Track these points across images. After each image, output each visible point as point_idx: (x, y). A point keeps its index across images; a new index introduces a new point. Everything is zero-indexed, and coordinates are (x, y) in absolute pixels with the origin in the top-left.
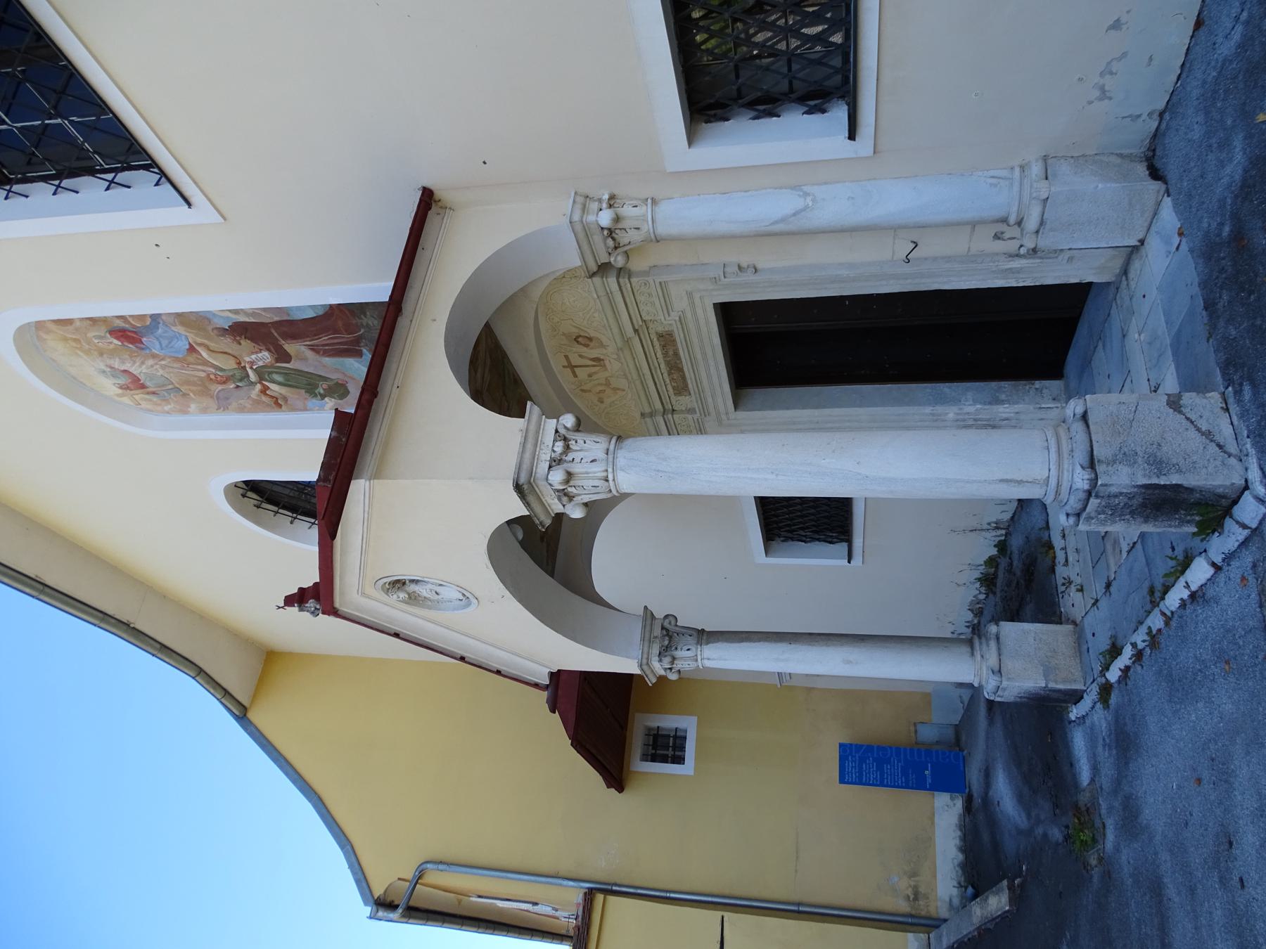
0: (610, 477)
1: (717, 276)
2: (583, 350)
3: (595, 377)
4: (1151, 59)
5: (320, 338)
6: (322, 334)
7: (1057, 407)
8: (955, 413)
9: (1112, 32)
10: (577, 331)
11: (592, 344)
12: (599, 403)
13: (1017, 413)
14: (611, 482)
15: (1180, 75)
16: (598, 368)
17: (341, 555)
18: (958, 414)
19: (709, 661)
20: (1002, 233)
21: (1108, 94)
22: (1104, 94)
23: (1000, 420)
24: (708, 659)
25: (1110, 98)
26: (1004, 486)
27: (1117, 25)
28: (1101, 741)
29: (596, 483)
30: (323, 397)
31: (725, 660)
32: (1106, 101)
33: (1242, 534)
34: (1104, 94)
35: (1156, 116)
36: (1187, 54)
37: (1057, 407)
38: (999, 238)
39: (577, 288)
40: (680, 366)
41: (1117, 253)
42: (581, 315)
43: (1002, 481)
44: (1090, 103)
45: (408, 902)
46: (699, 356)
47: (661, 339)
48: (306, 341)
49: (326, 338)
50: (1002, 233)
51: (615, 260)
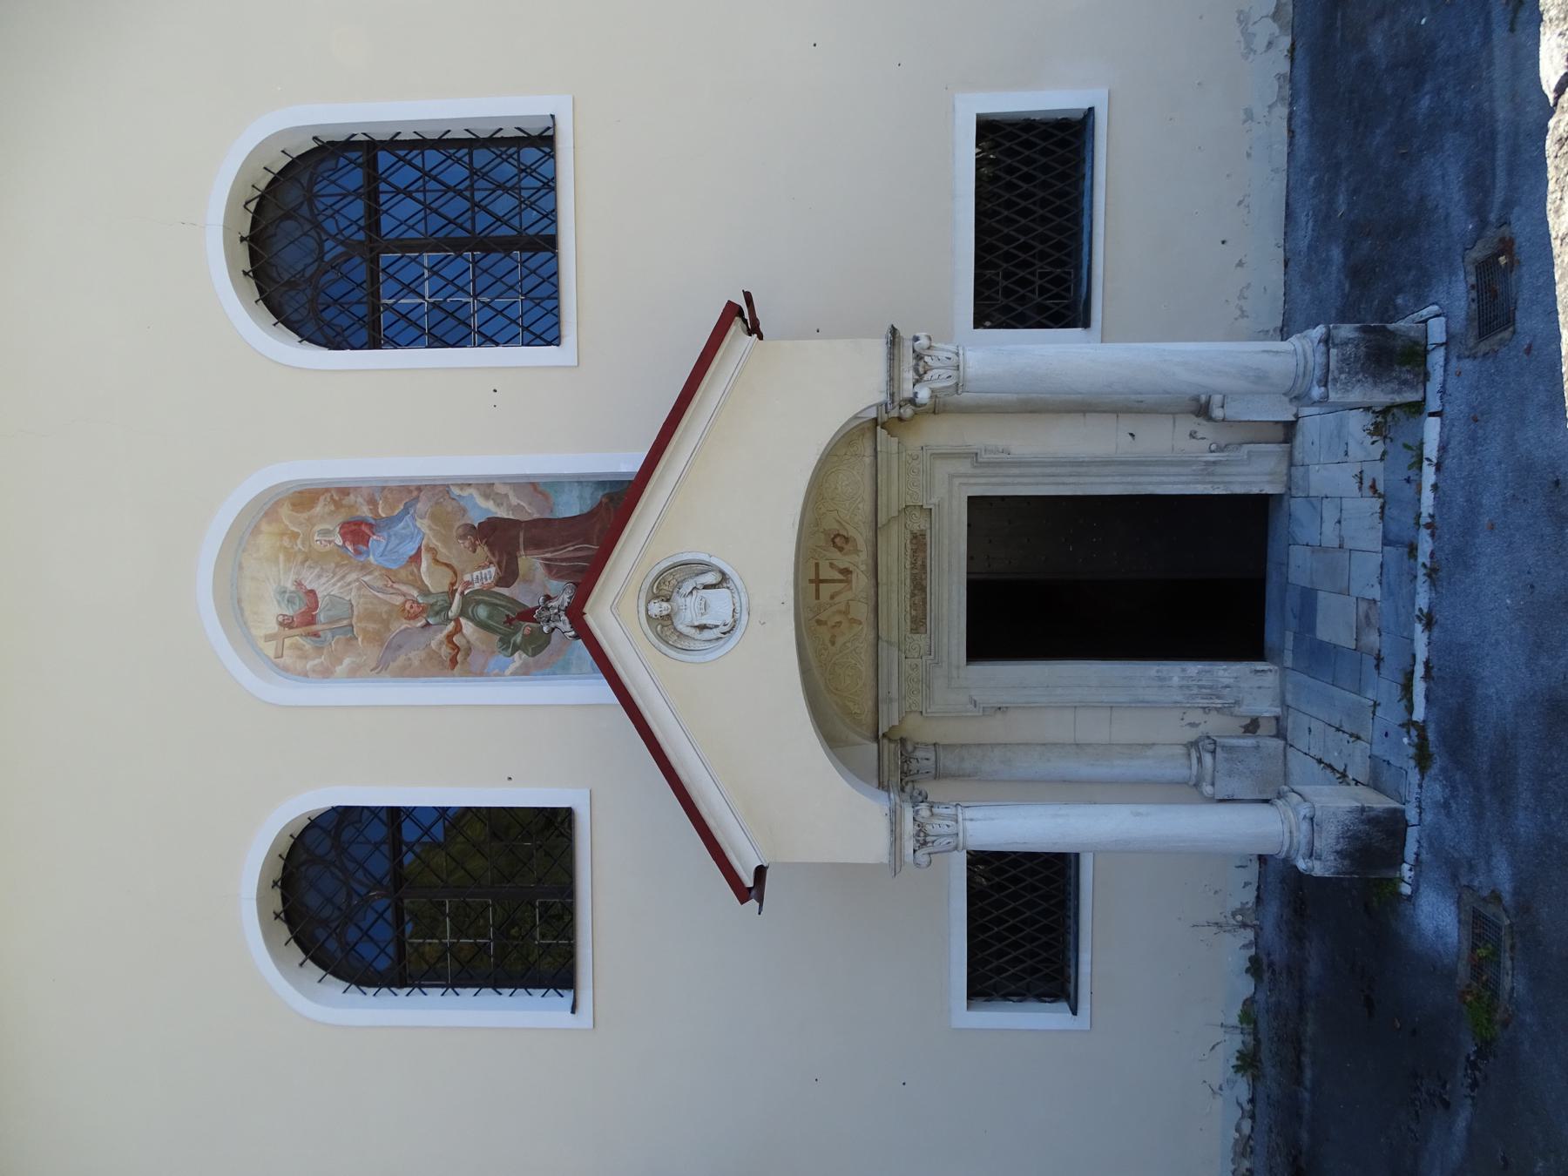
0: (961, 352)
1: (979, 451)
2: (837, 554)
3: (837, 600)
4: (1265, 289)
5: (565, 548)
6: (569, 542)
7: (1271, 671)
8: (1179, 677)
9: (1239, 268)
10: (838, 528)
11: (847, 547)
12: (829, 645)
13: (1236, 678)
14: (961, 356)
15: (1285, 300)
16: (842, 585)
17: (664, 467)
18: (1183, 678)
19: (973, 822)
20: (1195, 432)
21: (1245, 314)
22: (1243, 314)
23: (1222, 687)
24: (971, 820)
25: (1248, 317)
26: (1266, 355)
27: (1240, 264)
28: (1463, 1059)
29: (950, 355)
30: (516, 648)
31: (993, 819)
32: (1245, 319)
33: (1441, 352)
34: (1243, 314)
35: (1278, 333)
36: (1285, 285)
37: (1271, 671)
38: (1194, 438)
39: (853, 469)
40: (924, 582)
41: (1279, 449)
42: (847, 505)
43: (1264, 351)
44: (1236, 319)
45: (575, 993)
46: (946, 566)
47: (914, 541)
48: (547, 552)
49: (572, 548)
50: (1195, 432)
51: (904, 411)
